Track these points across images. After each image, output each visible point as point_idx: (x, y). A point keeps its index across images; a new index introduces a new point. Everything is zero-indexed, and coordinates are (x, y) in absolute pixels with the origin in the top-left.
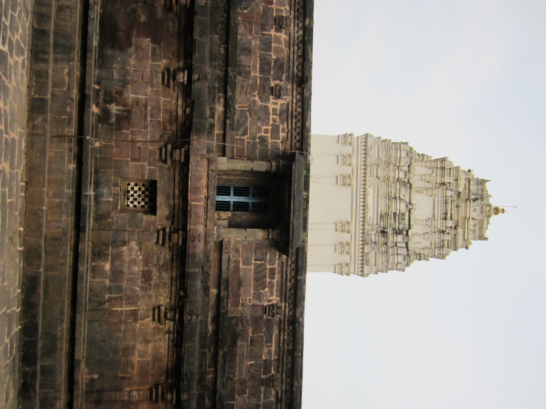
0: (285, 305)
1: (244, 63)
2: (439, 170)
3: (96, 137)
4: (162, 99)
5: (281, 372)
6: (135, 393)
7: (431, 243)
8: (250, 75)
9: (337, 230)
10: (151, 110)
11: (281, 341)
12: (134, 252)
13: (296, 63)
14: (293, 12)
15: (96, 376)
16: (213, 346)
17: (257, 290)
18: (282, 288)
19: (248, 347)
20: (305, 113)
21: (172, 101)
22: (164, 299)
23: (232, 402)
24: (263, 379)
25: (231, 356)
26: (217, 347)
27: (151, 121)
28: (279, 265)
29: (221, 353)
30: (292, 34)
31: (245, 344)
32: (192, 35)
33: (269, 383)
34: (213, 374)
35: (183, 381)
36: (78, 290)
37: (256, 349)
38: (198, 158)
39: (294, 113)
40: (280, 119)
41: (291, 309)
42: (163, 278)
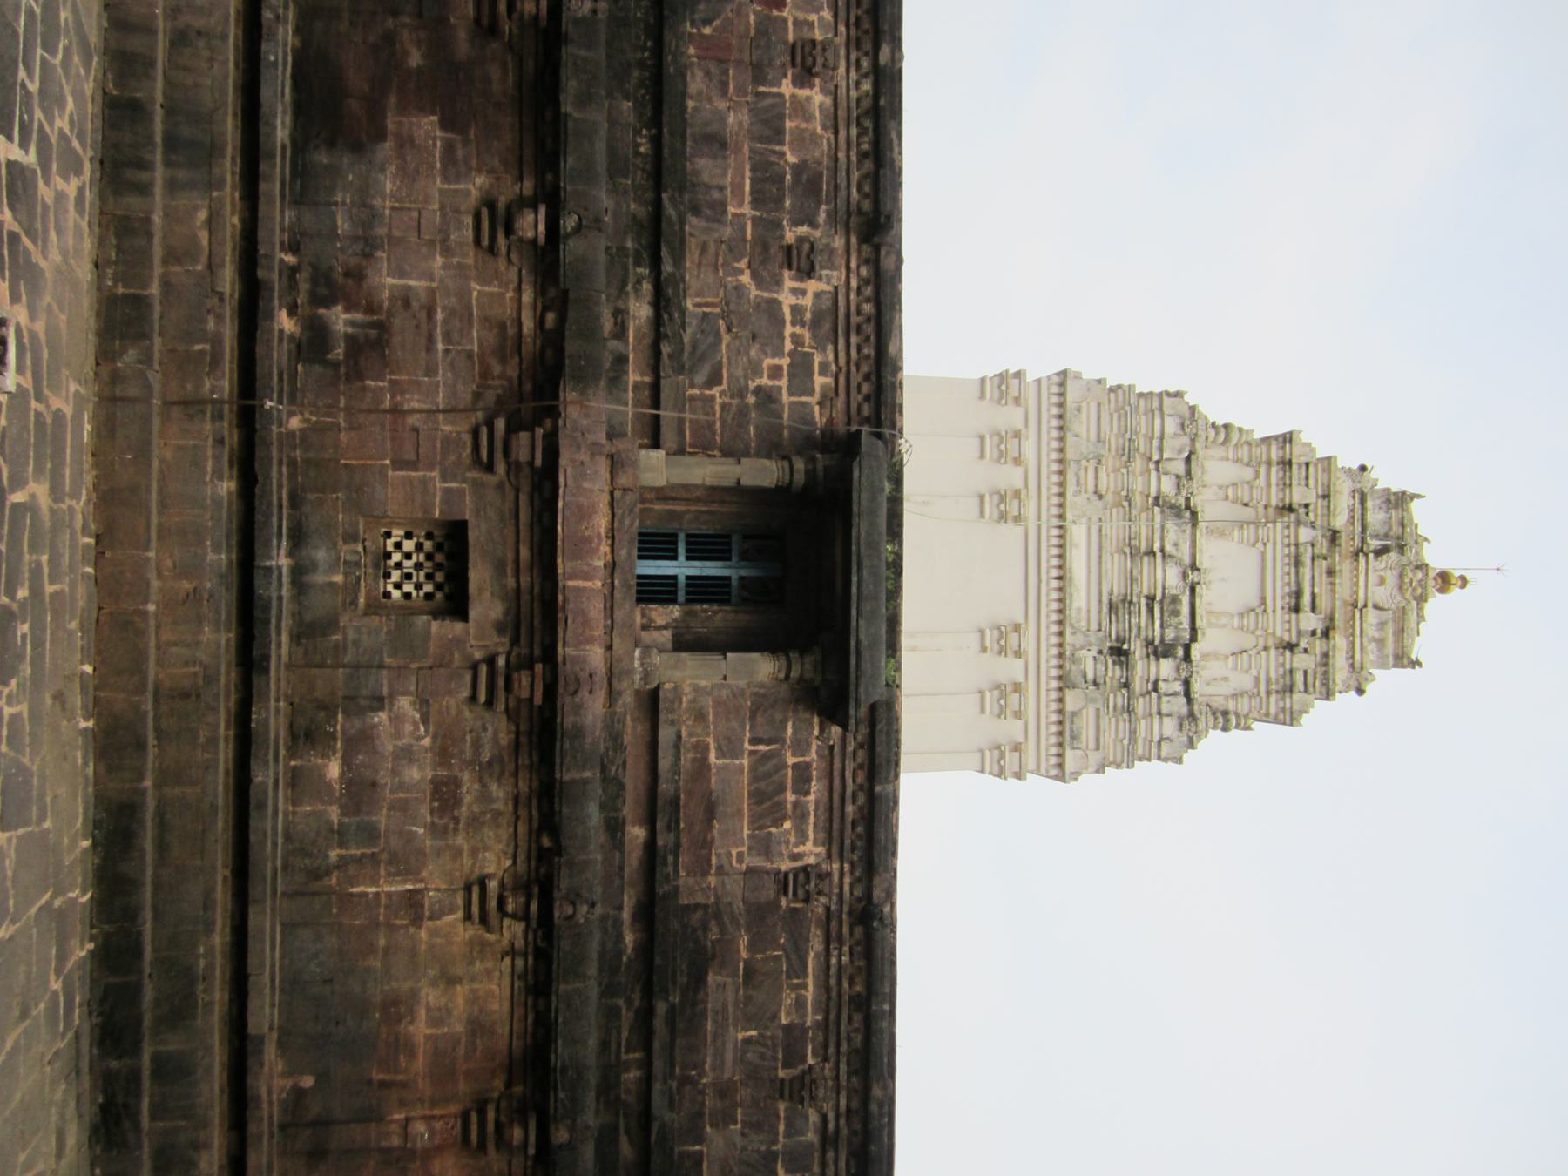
0: (842, 868)
1: (705, 178)
2: (1274, 469)
4: (476, 288)
5: (833, 1060)
6: (420, 1127)
7: (1257, 679)
8: (725, 212)
9: (984, 649)
10: (445, 322)
11: (833, 970)
12: (408, 728)
14: (842, 29)
15: (308, 1082)
16: (638, 988)
17: (761, 828)
18: (831, 820)
21: (502, 294)
22: (495, 859)
23: (697, 1148)
24: (782, 1081)
25: (688, 1018)
26: (648, 992)
27: (447, 351)
29: (661, 1008)
30: (842, 91)
31: (729, 980)
32: (556, 103)
33: (800, 1090)
35: (556, 1089)
36: (252, 838)
39: (855, 319)
40: (814, 337)
41: (859, 880)
42: (493, 801)
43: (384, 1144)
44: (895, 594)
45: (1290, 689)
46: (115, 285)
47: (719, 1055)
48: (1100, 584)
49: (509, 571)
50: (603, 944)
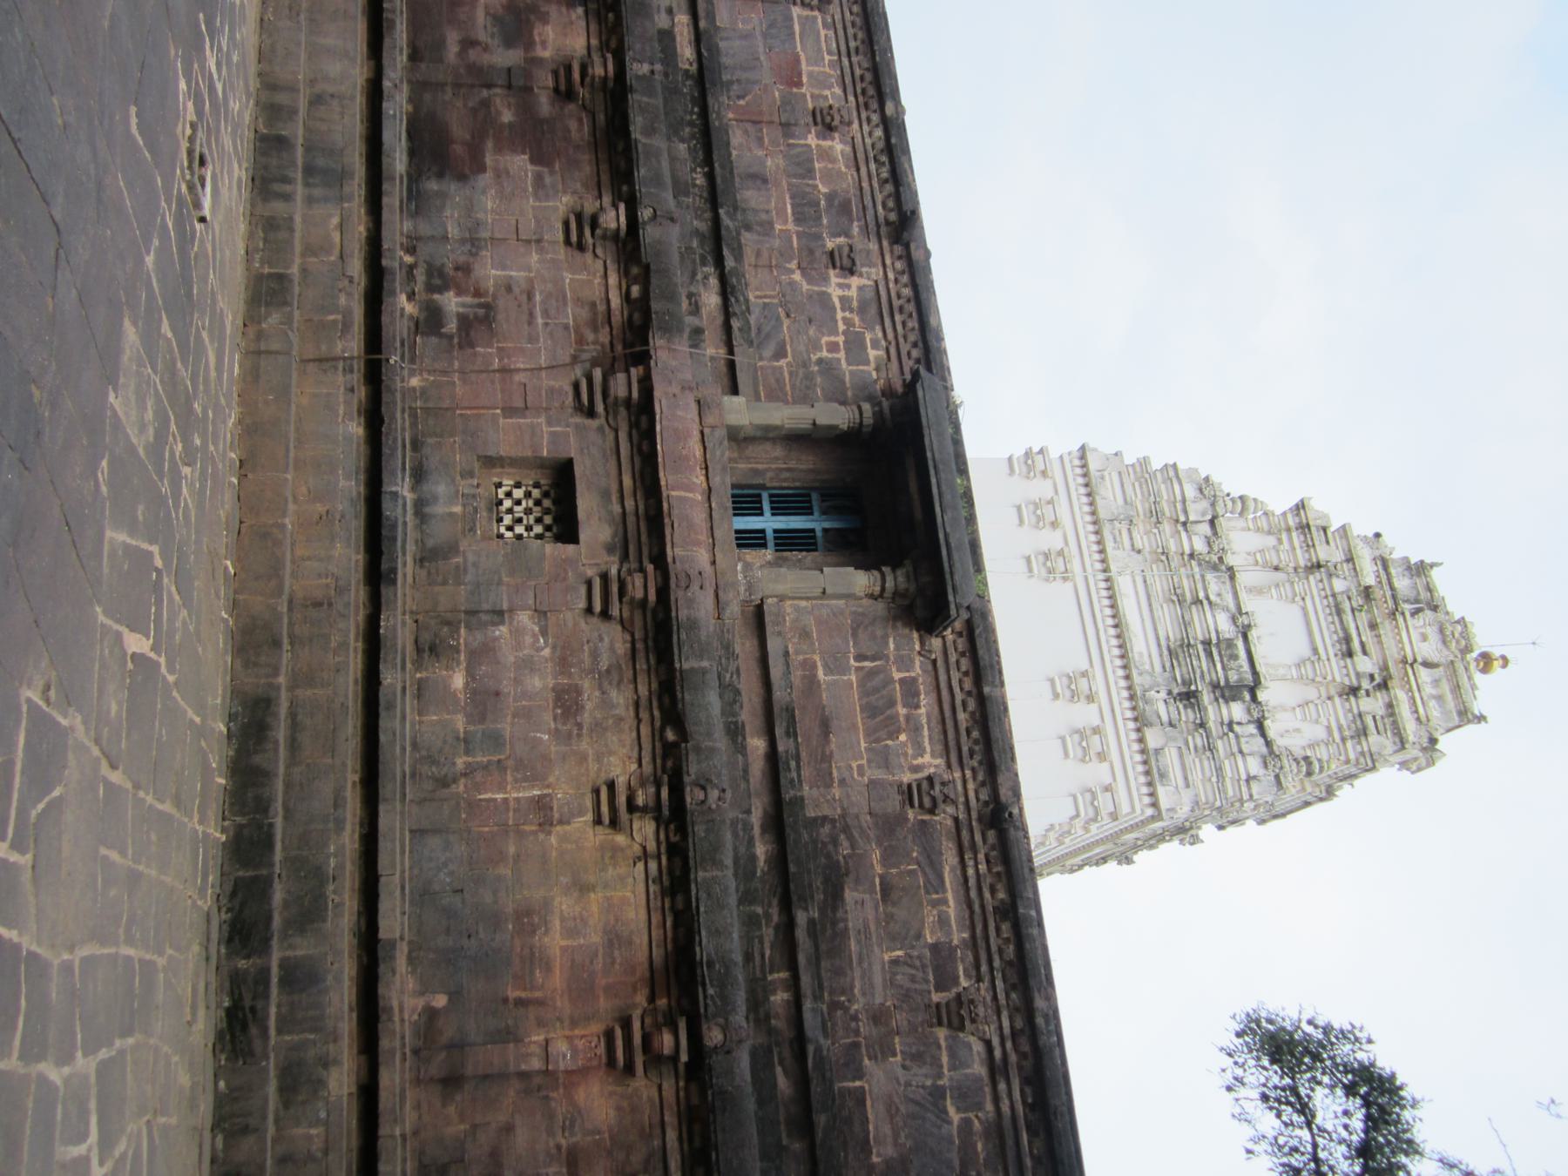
0: (964, 775)
1: (753, 204)
2: (1294, 534)
3: (412, 361)
4: (568, 277)
5: (987, 979)
6: (561, 1046)
7: (1329, 728)
8: (772, 228)
9: (1056, 696)
10: (543, 302)
11: (972, 882)
12: (528, 640)
13: (879, 198)
14: (851, 98)
15: (440, 1001)
16: (775, 902)
17: (877, 741)
18: (945, 732)
19: (877, 909)
20: (923, 296)
21: (594, 280)
22: (621, 759)
23: (858, 1083)
24: (938, 1005)
25: (829, 933)
26: (787, 906)
27: (546, 324)
28: (924, 671)
29: (801, 918)
30: (858, 140)
31: (867, 897)
32: (627, 134)
33: (956, 1015)
34: (787, 989)
35: (704, 985)
36: (382, 738)
37: (901, 913)
38: (675, 389)
39: (896, 303)
40: (862, 320)
41: (983, 784)
42: (613, 706)
43: (523, 1067)
44: (971, 519)
45: (1363, 732)
46: (262, 266)
47: (867, 976)
48: (1156, 629)
49: (615, 497)
50: (735, 849)
